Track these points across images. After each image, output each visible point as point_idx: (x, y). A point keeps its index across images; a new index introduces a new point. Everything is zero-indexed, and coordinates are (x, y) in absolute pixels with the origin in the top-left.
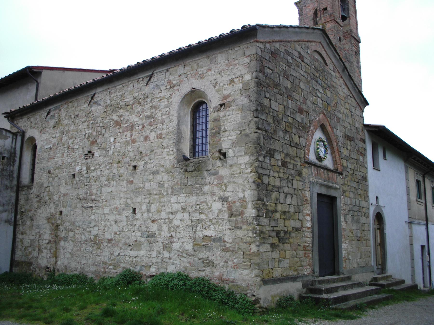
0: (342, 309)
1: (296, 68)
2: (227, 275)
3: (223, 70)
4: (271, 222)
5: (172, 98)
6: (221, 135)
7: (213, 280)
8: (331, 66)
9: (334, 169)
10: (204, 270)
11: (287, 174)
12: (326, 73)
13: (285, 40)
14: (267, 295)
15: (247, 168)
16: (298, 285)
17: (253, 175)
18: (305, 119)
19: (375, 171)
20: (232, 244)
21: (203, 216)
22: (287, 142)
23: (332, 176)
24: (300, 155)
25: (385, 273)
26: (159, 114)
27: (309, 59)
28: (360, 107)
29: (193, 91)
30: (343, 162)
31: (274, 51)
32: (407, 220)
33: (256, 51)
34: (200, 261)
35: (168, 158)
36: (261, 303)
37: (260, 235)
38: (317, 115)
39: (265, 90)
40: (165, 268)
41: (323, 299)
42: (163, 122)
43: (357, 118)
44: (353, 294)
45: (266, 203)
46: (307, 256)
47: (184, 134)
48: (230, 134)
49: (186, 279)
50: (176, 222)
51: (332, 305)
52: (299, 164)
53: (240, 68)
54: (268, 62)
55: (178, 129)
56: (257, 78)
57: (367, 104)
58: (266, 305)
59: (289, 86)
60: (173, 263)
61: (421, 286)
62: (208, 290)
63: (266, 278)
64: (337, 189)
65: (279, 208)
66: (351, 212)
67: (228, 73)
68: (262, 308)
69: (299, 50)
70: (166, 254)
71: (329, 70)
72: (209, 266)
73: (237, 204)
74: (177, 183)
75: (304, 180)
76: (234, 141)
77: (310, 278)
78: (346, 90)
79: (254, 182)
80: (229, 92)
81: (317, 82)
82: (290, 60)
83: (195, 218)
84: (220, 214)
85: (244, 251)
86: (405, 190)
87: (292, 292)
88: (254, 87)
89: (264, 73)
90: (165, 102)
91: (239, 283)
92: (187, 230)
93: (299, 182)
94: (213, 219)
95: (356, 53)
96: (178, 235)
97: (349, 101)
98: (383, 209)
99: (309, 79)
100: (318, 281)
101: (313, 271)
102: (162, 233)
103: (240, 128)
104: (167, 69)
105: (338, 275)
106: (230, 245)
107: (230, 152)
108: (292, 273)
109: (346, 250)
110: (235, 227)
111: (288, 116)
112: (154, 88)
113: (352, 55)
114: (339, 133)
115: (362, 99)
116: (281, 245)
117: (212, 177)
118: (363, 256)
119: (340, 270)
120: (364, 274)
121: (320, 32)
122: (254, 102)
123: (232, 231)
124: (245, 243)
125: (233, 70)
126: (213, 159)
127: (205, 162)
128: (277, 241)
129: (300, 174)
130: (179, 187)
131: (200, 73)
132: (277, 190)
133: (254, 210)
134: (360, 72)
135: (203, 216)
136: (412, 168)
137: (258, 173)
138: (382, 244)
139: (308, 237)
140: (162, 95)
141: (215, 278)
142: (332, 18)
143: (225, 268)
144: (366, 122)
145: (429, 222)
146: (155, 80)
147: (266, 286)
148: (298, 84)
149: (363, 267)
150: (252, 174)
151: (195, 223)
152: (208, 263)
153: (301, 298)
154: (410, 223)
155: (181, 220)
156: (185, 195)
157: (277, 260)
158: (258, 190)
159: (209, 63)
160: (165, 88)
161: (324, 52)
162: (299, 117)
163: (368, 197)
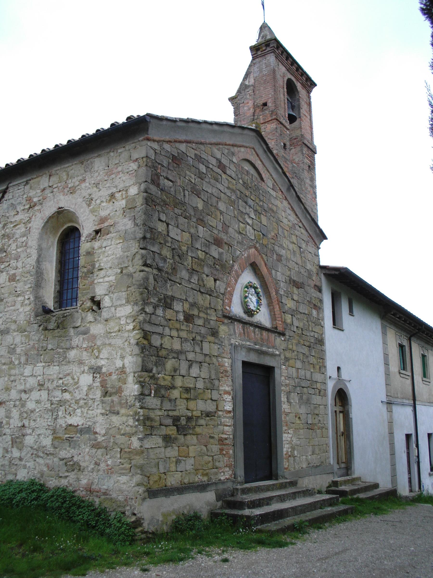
0: (269, 531)
1: (212, 181)
2: (98, 484)
3: (100, 180)
4: (164, 404)
5: (32, 222)
6: (95, 275)
7: (78, 492)
8: (270, 183)
9: (273, 328)
10: (66, 477)
11: (192, 332)
12: (261, 192)
13: (195, 140)
14: (155, 513)
15: (128, 324)
16: (210, 496)
17: (137, 334)
18: (225, 254)
19: (336, 331)
20: (106, 437)
21: (67, 396)
22: (194, 286)
23: (268, 337)
24: (215, 306)
25: (351, 475)
26: (14, 246)
27: (235, 170)
28: (314, 241)
29: (61, 214)
30: (286, 318)
31: (176, 155)
32: (385, 400)
33: (147, 153)
34: (61, 462)
35: (22, 310)
36: (144, 525)
37: (145, 423)
38: (245, 250)
39: (160, 209)
40: (14, 474)
41: (242, 516)
42: (17, 259)
43: (309, 256)
44: (292, 508)
45: (156, 375)
46: (224, 452)
47: (46, 275)
48: (107, 273)
49: (41, 490)
50: (31, 405)
51: (256, 524)
52: (215, 318)
53: (124, 178)
54: (166, 170)
55: (37, 267)
56: (146, 192)
57: (324, 237)
58: (152, 529)
59: (200, 206)
60: (25, 467)
61: (404, 490)
62: (70, 507)
63: (155, 487)
64: (276, 355)
65: (179, 382)
66: (298, 388)
67: (107, 185)
68: (146, 532)
69: (219, 156)
70: (16, 453)
71: (266, 187)
72: (73, 470)
73: (114, 377)
74: (33, 347)
75: (222, 342)
76: (112, 284)
77: (229, 485)
78: (292, 218)
79: (137, 344)
80: (108, 213)
81: (246, 203)
82: (203, 169)
83: (56, 399)
84: (91, 393)
85: (122, 446)
86: (382, 357)
87: (198, 507)
88: (142, 205)
89: (158, 185)
90: (22, 229)
91: (114, 495)
92: (45, 416)
93: (212, 344)
94: (80, 399)
95: (309, 167)
96: (32, 424)
97: (297, 233)
98: (348, 384)
99: (233, 197)
100: (241, 489)
101: (235, 474)
102: (12, 421)
103: (121, 264)
104: (27, 181)
105: (277, 479)
106: (103, 438)
107: (106, 300)
108: (199, 478)
109: (290, 443)
110: (110, 412)
111: (197, 249)
112: (8, 208)
113: (303, 170)
114: (279, 276)
115: (317, 230)
116: (181, 437)
117: (81, 337)
118: (317, 451)
119: (279, 472)
120: (318, 476)
121: (253, 134)
122: (141, 226)
123: (106, 417)
124: (123, 435)
125: (114, 180)
126: (83, 311)
127: (71, 315)
128: (175, 432)
129: (214, 333)
130: (36, 352)
131: (69, 186)
132: (175, 355)
133: (136, 386)
134: (315, 193)
135: (67, 396)
136: (392, 327)
137: (143, 330)
138: (346, 434)
139: (227, 426)
140: (18, 218)
141: (81, 489)
142: (274, 117)
143: (95, 474)
144: (323, 263)
145: (417, 403)
146: (11, 197)
147: (155, 500)
148: (215, 204)
149: (317, 466)
150: (135, 332)
151: (56, 405)
152: (72, 465)
153: (213, 515)
154: (389, 403)
155: (38, 402)
156: (44, 364)
157: (174, 460)
158: (142, 355)
159: (83, 171)
160: (22, 208)
161: (259, 162)
162: (214, 251)
163: (325, 367)
